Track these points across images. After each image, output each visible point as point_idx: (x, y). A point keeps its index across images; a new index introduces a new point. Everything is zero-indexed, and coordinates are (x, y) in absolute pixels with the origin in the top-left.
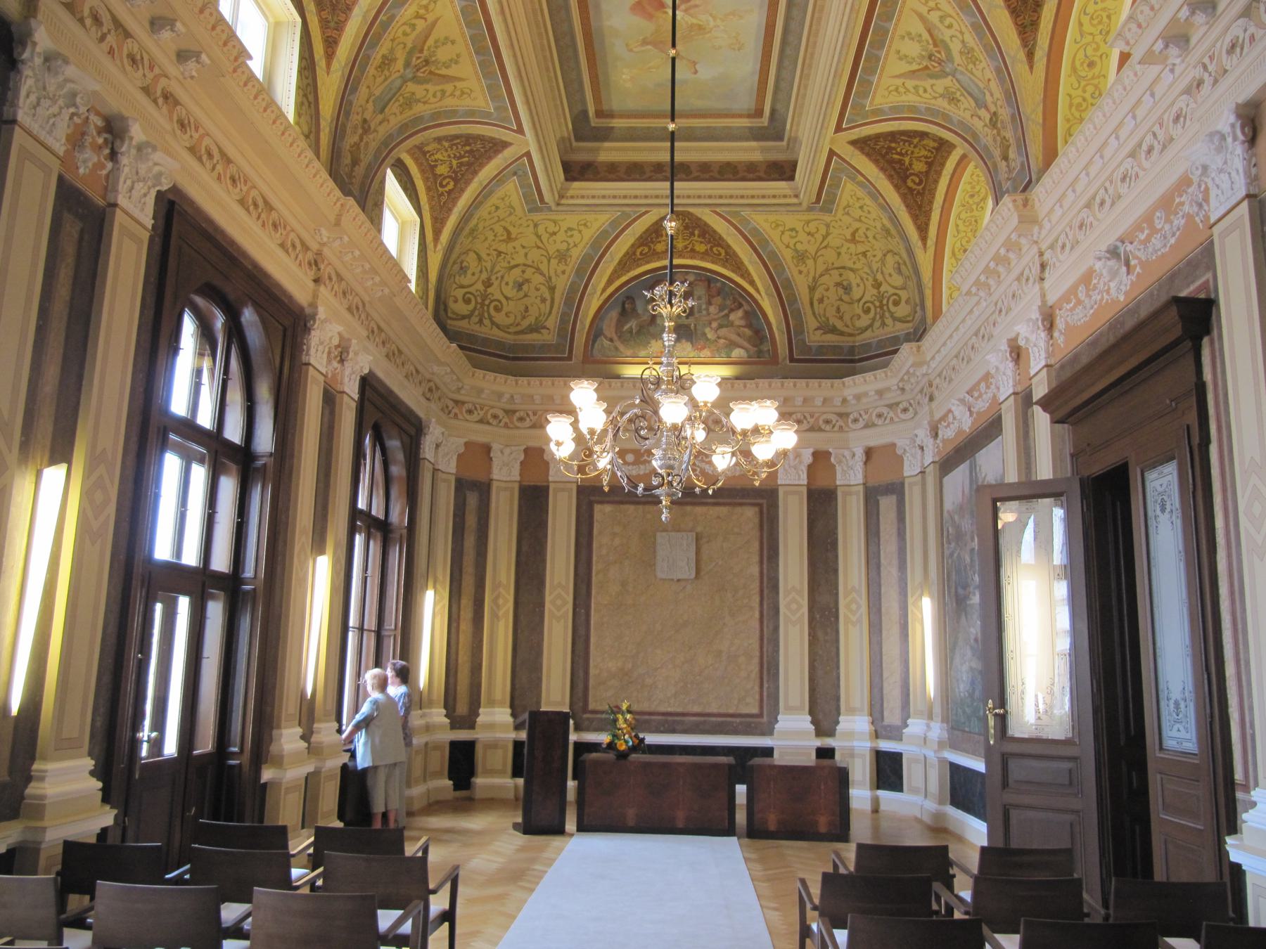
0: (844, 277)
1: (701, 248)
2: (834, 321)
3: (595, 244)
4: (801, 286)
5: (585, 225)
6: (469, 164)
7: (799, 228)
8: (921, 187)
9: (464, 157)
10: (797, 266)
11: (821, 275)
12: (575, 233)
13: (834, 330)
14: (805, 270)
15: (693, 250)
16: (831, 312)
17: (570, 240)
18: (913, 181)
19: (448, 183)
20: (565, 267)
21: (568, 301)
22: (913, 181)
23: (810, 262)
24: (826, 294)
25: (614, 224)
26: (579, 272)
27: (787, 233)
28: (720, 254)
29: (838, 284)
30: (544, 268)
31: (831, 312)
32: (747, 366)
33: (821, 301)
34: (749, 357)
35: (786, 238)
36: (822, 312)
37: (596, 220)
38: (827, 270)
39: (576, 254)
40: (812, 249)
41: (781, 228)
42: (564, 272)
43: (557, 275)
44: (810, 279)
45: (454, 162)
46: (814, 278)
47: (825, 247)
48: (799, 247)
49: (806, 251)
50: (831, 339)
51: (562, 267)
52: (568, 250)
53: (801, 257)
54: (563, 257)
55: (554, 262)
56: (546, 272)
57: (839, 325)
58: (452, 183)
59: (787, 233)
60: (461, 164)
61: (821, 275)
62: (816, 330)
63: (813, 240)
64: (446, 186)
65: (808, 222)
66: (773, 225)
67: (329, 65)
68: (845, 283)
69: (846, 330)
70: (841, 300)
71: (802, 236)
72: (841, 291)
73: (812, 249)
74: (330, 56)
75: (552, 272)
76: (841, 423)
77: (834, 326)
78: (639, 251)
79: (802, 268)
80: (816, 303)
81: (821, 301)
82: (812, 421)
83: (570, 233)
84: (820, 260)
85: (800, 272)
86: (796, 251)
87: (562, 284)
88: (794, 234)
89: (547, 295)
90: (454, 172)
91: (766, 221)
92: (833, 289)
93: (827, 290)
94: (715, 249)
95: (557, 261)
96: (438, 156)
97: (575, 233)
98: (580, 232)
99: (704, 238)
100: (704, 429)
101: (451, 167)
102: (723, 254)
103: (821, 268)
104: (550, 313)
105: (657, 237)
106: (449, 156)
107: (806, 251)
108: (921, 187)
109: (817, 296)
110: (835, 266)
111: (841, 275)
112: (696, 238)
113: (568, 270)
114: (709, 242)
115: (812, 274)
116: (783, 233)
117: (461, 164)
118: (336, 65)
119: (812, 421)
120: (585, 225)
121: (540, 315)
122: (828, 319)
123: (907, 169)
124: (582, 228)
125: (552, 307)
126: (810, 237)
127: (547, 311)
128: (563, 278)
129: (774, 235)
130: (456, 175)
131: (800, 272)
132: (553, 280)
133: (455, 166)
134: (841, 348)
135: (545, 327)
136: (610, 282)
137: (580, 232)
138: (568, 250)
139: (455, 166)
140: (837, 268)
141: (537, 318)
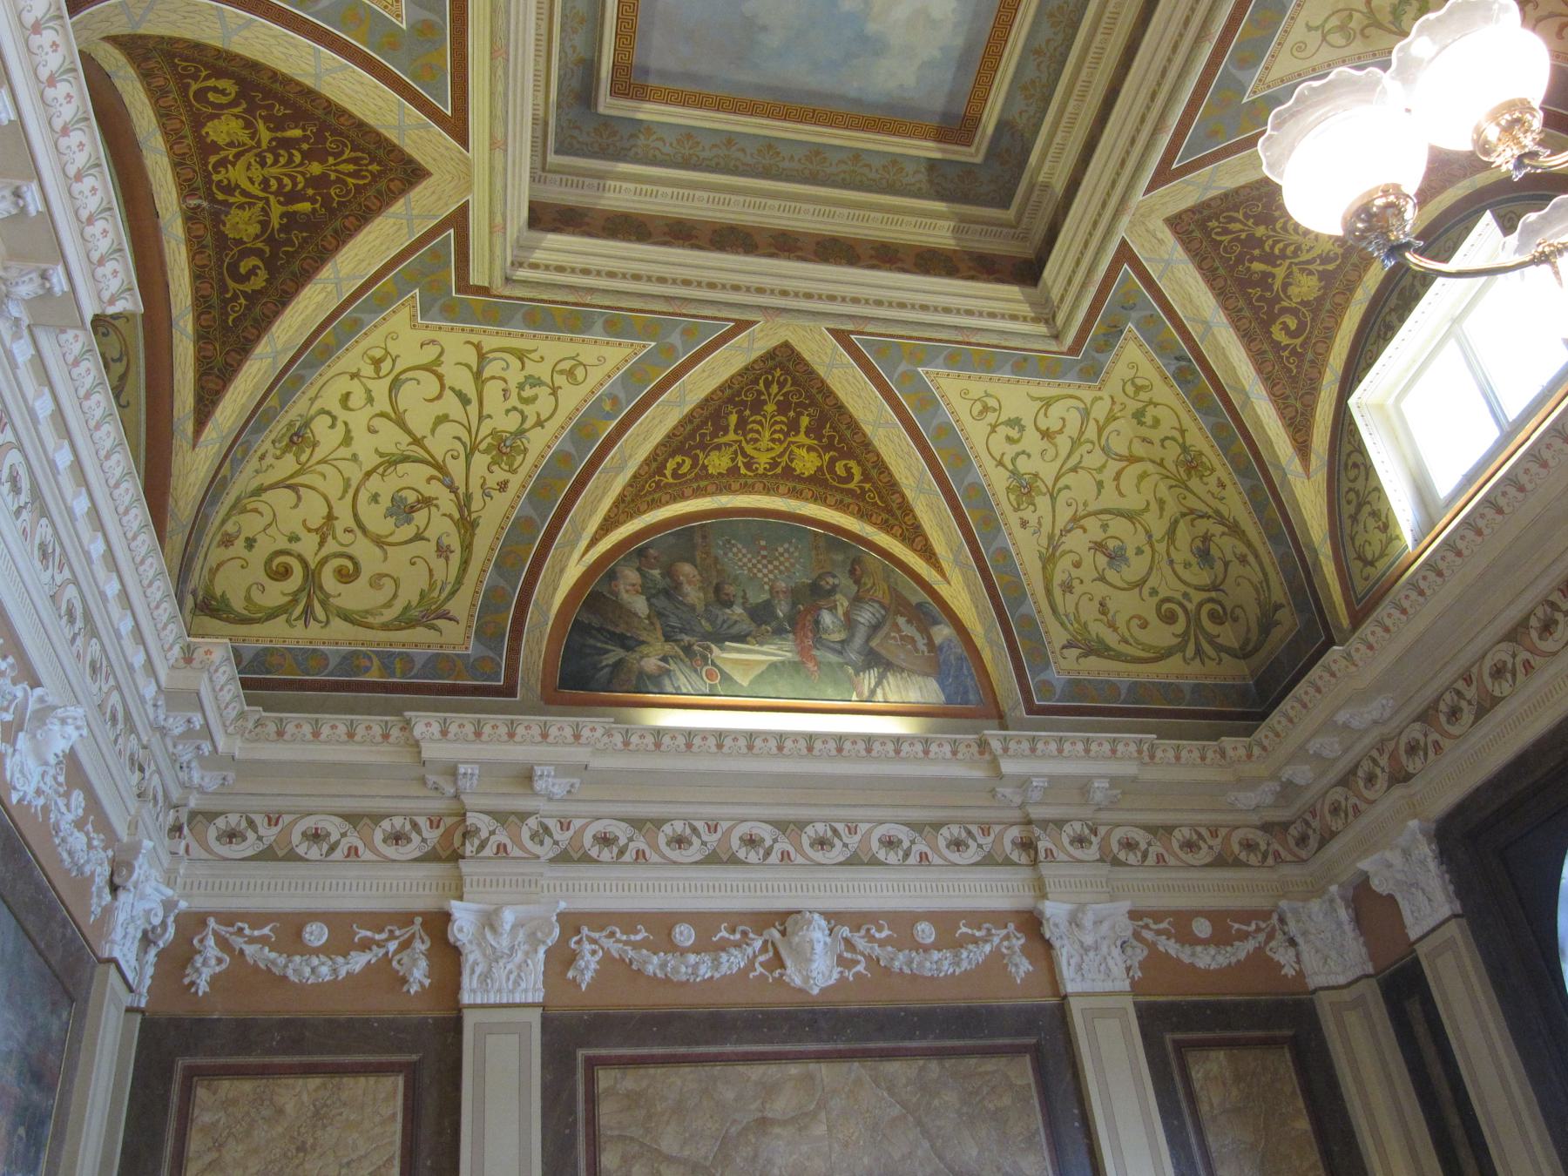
0: (1110, 532)
1: (807, 463)
2: (1098, 629)
3: (581, 430)
4: (1026, 548)
5: (570, 373)
6: (311, 225)
7: (1028, 422)
8: (1298, 341)
9: (304, 199)
10: (1016, 510)
11: (1066, 531)
12: (543, 392)
13: (1096, 649)
14: (1033, 521)
15: (788, 472)
16: (1089, 612)
17: (528, 409)
18: (1285, 327)
19: (253, 272)
20: (507, 476)
21: (505, 561)
22: (1285, 327)
23: (1043, 502)
24: (1075, 573)
25: (633, 376)
26: (540, 490)
27: (1003, 431)
28: (850, 477)
29: (1099, 546)
30: (456, 468)
31: (1089, 612)
32: (940, 720)
33: (1068, 588)
34: (949, 700)
35: (998, 444)
36: (1071, 610)
37: (602, 360)
38: (1075, 519)
39: (539, 443)
40: (1048, 471)
41: (991, 417)
42: (503, 486)
43: (486, 494)
44: (1044, 542)
45: (276, 210)
46: (1051, 537)
47: (1074, 469)
48: (1024, 466)
49: (1036, 475)
50: (1095, 667)
51: (500, 474)
52: (520, 433)
53: (1025, 489)
54: (505, 448)
55: (481, 461)
56: (459, 482)
57: (1111, 639)
58: (263, 274)
59: (1003, 431)
60: (291, 220)
61: (1066, 531)
62: (1064, 647)
63: (1051, 452)
64: (244, 279)
65: (1048, 403)
66: (978, 407)
67: (198, 432)
68: (1111, 544)
69: (1123, 648)
70: (1102, 579)
71: (1031, 441)
72: (1102, 560)
73: (1048, 471)
74: (204, 411)
75: (475, 489)
76: (784, 845)
77: (1100, 641)
78: (671, 465)
79: (1027, 514)
80: (1057, 592)
81: (1068, 588)
82: (712, 838)
83: (528, 392)
84: (1063, 497)
85: (1024, 524)
86: (1014, 473)
87: (493, 516)
88: (1014, 434)
89: (454, 542)
90: (271, 240)
91: (964, 394)
92: (1088, 558)
93: (1077, 565)
94: (839, 468)
95: (487, 459)
96: (236, 174)
97: (543, 392)
98: (554, 391)
99: (819, 438)
100: (1230, 964)
101: (264, 224)
102: (857, 477)
103: (1064, 515)
104: (459, 581)
105: (714, 435)
106: (265, 183)
107: (1036, 475)
108: (1298, 341)
109: (1058, 578)
110: (1091, 508)
111: (1105, 527)
112: (802, 438)
113: (515, 482)
114: (829, 447)
115: (1046, 528)
116: (993, 429)
117: (291, 220)
118: (210, 433)
119: (712, 838)
120: (570, 373)
121: (432, 585)
122: (1085, 625)
123: (1278, 299)
124: (560, 380)
125: (465, 563)
126: (1045, 444)
127: (452, 579)
128: (502, 501)
129: (975, 433)
130: (274, 255)
131: (1024, 524)
132: (475, 505)
133: (275, 222)
134: (1113, 686)
135: (446, 616)
136: (607, 526)
137: (554, 391)
138: (520, 433)
139: (275, 222)
140: (1095, 513)
141: (422, 595)
